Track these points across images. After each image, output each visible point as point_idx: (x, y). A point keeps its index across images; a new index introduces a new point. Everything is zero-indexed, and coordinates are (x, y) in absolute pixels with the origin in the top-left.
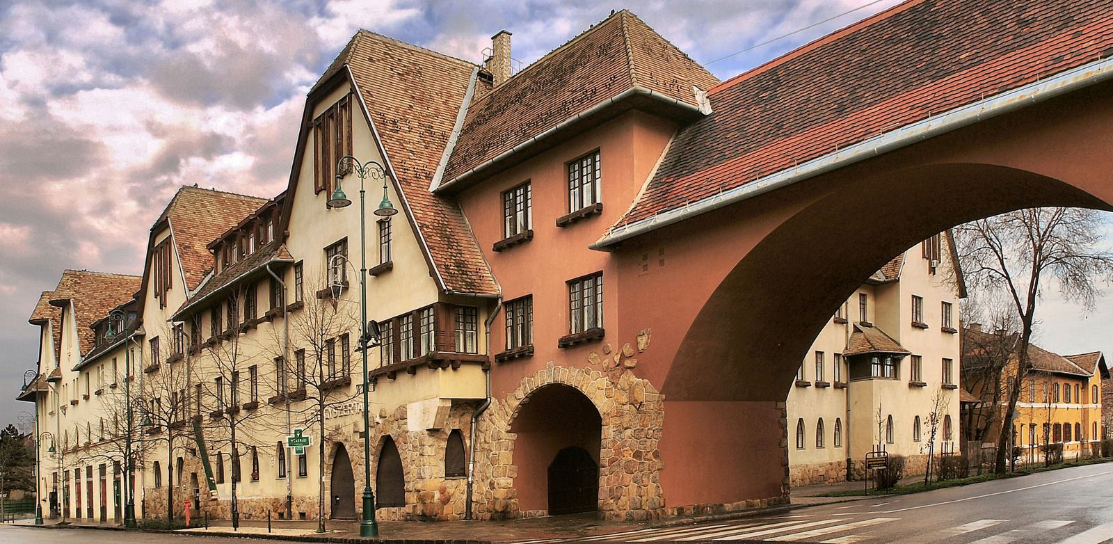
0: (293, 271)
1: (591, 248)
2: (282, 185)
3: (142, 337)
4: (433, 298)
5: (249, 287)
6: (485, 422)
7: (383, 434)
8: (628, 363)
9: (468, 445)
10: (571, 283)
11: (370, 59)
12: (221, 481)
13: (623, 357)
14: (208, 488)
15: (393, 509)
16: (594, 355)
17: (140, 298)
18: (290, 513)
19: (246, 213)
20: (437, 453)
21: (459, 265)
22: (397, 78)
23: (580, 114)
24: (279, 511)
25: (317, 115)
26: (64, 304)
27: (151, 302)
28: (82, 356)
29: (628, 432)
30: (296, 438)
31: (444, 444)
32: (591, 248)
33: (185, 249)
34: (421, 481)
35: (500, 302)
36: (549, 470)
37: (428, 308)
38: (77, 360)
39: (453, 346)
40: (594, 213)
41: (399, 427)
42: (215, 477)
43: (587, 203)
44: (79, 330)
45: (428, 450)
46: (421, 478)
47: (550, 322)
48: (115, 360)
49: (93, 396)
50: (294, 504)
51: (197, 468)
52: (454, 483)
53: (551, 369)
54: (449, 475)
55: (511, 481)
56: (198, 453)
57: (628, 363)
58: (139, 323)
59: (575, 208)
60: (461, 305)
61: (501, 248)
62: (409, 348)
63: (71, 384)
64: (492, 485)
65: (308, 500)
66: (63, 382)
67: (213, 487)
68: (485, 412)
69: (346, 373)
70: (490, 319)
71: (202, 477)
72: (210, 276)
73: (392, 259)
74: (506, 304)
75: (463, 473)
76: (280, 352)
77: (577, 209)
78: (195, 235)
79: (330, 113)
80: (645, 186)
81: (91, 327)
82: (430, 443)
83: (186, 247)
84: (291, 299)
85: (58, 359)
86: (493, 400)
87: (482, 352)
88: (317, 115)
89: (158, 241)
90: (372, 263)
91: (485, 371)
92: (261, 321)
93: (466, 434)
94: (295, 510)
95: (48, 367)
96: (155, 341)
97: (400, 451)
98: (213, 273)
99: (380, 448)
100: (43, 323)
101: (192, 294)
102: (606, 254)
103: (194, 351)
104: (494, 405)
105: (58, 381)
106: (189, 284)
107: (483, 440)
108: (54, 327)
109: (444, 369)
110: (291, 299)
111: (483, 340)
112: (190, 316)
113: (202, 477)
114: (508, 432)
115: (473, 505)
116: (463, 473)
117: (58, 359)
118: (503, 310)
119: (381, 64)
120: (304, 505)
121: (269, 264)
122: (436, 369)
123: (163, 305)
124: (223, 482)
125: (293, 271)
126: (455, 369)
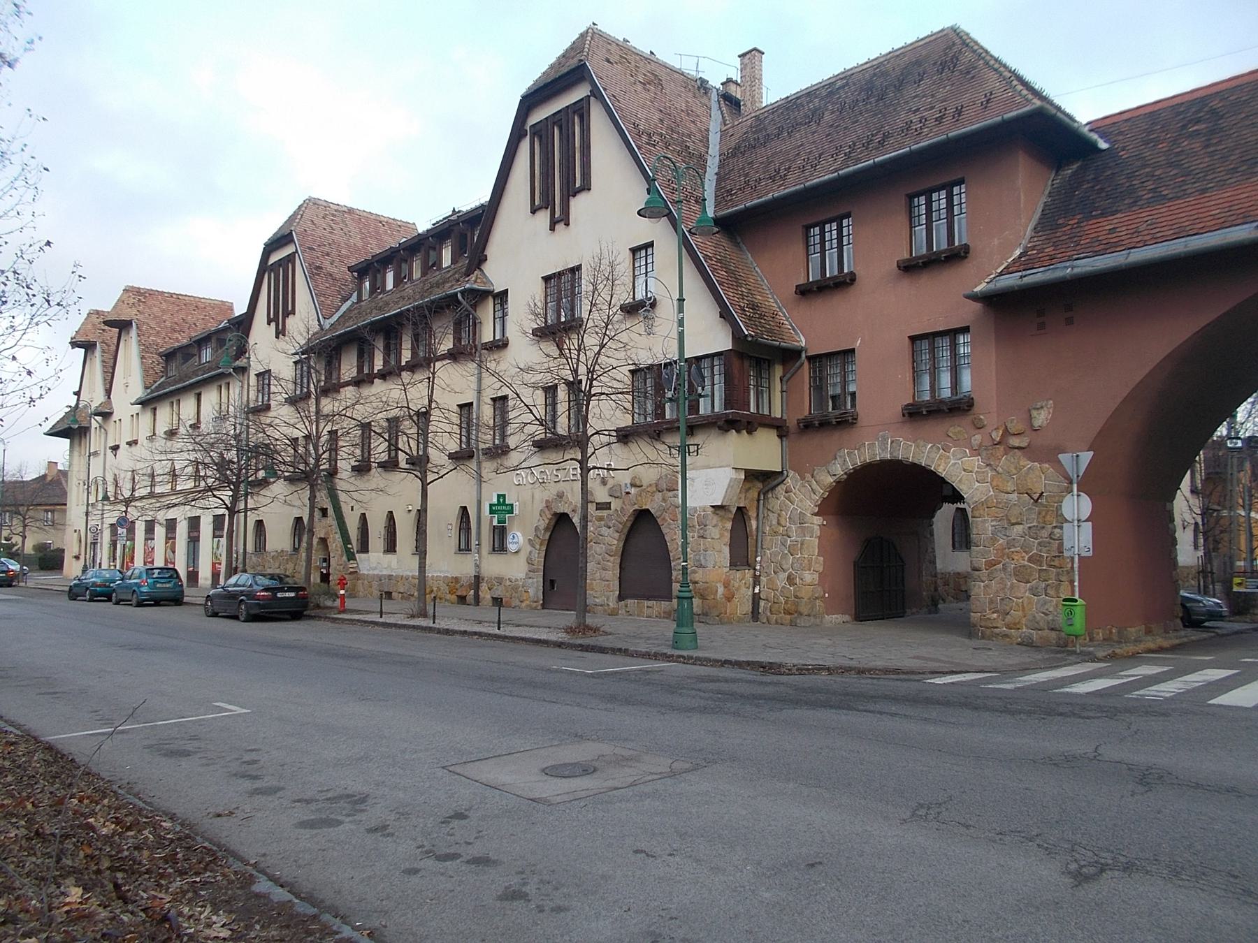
0: (490, 301)
1: (967, 297)
2: (485, 197)
3: (243, 370)
4: (721, 341)
5: (420, 320)
6: (778, 499)
7: (636, 507)
8: (1015, 442)
9: (754, 527)
10: (913, 339)
11: (608, 61)
12: (364, 548)
13: (1007, 433)
14: (345, 558)
15: (646, 603)
16: (956, 427)
17: (243, 324)
18: (477, 597)
19: (393, 242)
20: (722, 535)
21: (754, 307)
22: (639, 88)
23: (1006, 116)
24: (459, 593)
25: (271, 261)
26: (123, 326)
27: (261, 332)
28: (147, 388)
29: (1019, 528)
30: (499, 504)
31: (729, 525)
32: (967, 297)
33: (315, 271)
34: (700, 571)
35: (803, 355)
36: (856, 564)
37: (712, 356)
38: (138, 392)
39: (747, 405)
40: (956, 256)
41: (664, 500)
42: (355, 544)
43: (940, 244)
44: (143, 357)
45: (714, 532)
46: (701, 566)
47: (881, 386)
48: (155, 409)
49: (123, 446)
50: (484, 587)
51: (327, 533)
52: (739, 574)
53: (880, 441)
54: (733, 565)
55: (816, 576)
56: (331, 511)
57: (1015, 442)
58: (242, 351)
59: (921, 249)
60: (755, 356)
61: (805, 291)
62: (671, 405)
63: (126, 421)
64: (790, 579)
65: (508, 583)
66: (115, 417)
67: (351, 557)
68: (779, 488)
69: (366, 455)
70: (788, 375)
71: (335, 542)
72: (349, 303)
73: (508, 334)
74: (809, 358)
75: (749, 565)
76: (469, 397)
77: (836, 273)
78: (328, 254)
79: (556, 119)
80: (1030, 228)
81: (160, 355)
82: (714, 522)
83: (318, 268)
84: (487, 335)
85: (108, 392)
86: (791, 473)
87: (777, 413)
88: (271, 261)
89: (273, 259)
90: (622, 296)
91: (780, 437)
92: (347, 384)
93: (753, 514)
94: (486, 595)
95: (95, 397)
96: (264, 375)
97: (665, 530)
98: (354, 298)
99: (629, 524)
100: (88, 347)
101: (327, 324)
102: (977, 306)
103: (331, 389)
104: (792, 479)
105: (106, 415)
106: (324, 310)
107: (774, 522)
108: (103, 351)
109: (738, 431)
110: (487, 335)
111: (776, 397)
112: (325, 352)
113: (335, 542)
114: (816, 514)
115: (762, 603)
116: (749, 565)
117: (108, 392)
118: (806, 364)
119: (619, 67)
120: (500, 588)
121: (462, 292)
122: (727, 431)
123: (280, 333)
124: (367, 551)
125: (490, 301)
126: (750, 433)
